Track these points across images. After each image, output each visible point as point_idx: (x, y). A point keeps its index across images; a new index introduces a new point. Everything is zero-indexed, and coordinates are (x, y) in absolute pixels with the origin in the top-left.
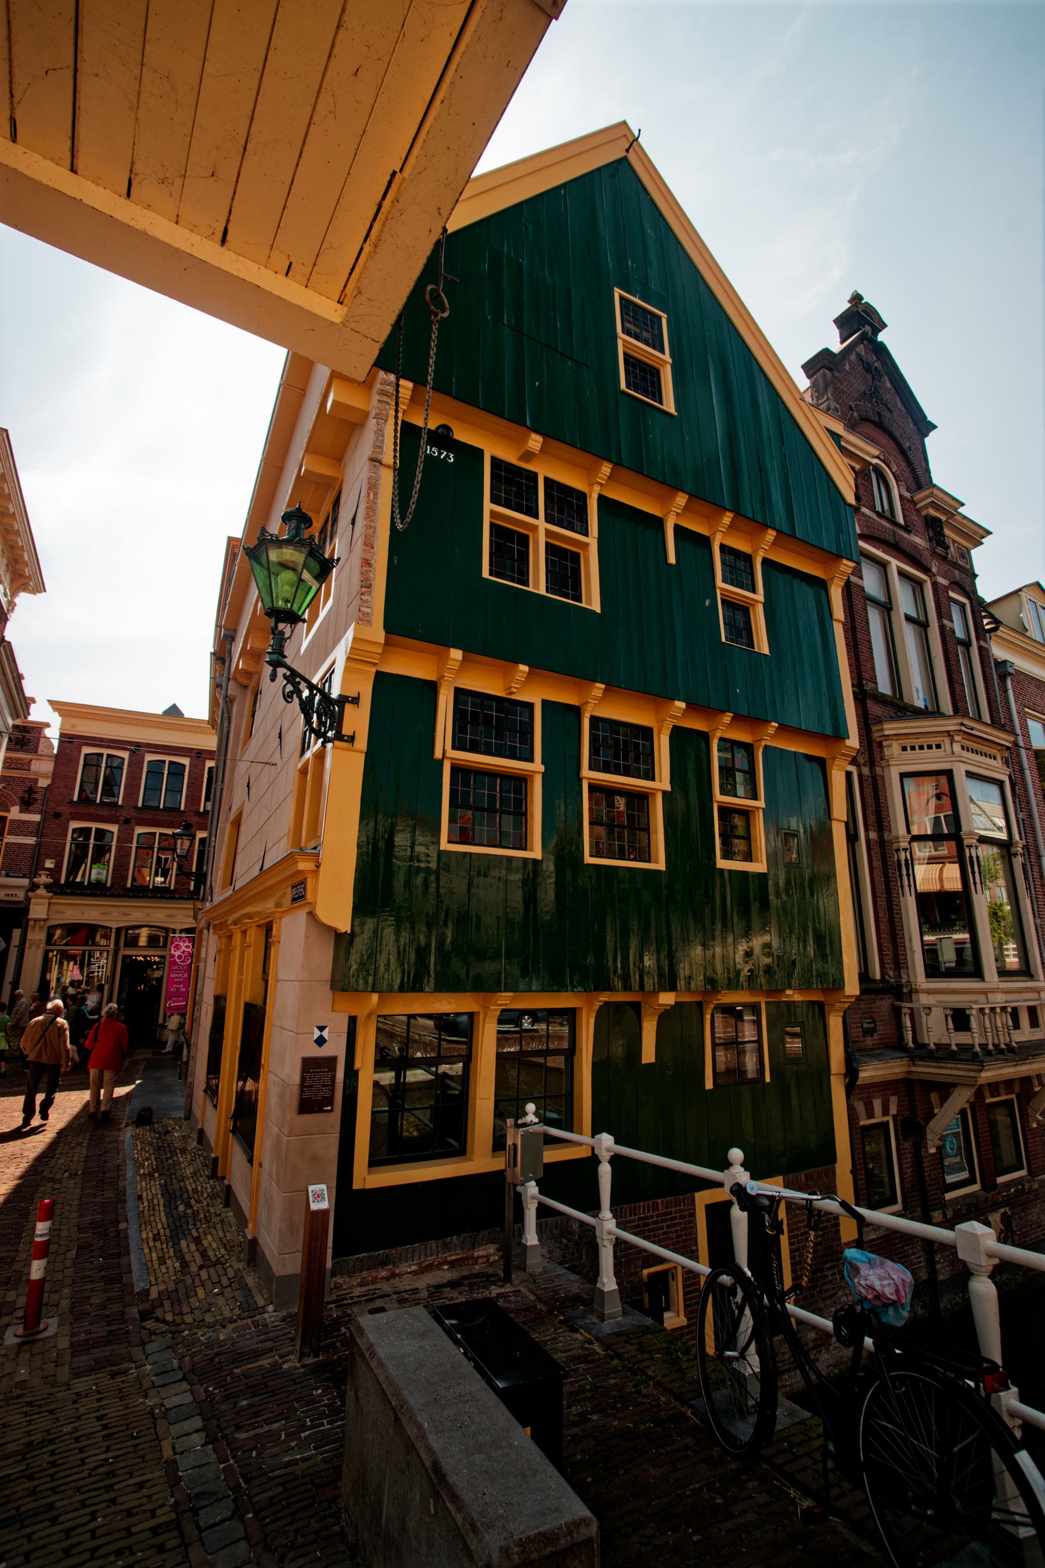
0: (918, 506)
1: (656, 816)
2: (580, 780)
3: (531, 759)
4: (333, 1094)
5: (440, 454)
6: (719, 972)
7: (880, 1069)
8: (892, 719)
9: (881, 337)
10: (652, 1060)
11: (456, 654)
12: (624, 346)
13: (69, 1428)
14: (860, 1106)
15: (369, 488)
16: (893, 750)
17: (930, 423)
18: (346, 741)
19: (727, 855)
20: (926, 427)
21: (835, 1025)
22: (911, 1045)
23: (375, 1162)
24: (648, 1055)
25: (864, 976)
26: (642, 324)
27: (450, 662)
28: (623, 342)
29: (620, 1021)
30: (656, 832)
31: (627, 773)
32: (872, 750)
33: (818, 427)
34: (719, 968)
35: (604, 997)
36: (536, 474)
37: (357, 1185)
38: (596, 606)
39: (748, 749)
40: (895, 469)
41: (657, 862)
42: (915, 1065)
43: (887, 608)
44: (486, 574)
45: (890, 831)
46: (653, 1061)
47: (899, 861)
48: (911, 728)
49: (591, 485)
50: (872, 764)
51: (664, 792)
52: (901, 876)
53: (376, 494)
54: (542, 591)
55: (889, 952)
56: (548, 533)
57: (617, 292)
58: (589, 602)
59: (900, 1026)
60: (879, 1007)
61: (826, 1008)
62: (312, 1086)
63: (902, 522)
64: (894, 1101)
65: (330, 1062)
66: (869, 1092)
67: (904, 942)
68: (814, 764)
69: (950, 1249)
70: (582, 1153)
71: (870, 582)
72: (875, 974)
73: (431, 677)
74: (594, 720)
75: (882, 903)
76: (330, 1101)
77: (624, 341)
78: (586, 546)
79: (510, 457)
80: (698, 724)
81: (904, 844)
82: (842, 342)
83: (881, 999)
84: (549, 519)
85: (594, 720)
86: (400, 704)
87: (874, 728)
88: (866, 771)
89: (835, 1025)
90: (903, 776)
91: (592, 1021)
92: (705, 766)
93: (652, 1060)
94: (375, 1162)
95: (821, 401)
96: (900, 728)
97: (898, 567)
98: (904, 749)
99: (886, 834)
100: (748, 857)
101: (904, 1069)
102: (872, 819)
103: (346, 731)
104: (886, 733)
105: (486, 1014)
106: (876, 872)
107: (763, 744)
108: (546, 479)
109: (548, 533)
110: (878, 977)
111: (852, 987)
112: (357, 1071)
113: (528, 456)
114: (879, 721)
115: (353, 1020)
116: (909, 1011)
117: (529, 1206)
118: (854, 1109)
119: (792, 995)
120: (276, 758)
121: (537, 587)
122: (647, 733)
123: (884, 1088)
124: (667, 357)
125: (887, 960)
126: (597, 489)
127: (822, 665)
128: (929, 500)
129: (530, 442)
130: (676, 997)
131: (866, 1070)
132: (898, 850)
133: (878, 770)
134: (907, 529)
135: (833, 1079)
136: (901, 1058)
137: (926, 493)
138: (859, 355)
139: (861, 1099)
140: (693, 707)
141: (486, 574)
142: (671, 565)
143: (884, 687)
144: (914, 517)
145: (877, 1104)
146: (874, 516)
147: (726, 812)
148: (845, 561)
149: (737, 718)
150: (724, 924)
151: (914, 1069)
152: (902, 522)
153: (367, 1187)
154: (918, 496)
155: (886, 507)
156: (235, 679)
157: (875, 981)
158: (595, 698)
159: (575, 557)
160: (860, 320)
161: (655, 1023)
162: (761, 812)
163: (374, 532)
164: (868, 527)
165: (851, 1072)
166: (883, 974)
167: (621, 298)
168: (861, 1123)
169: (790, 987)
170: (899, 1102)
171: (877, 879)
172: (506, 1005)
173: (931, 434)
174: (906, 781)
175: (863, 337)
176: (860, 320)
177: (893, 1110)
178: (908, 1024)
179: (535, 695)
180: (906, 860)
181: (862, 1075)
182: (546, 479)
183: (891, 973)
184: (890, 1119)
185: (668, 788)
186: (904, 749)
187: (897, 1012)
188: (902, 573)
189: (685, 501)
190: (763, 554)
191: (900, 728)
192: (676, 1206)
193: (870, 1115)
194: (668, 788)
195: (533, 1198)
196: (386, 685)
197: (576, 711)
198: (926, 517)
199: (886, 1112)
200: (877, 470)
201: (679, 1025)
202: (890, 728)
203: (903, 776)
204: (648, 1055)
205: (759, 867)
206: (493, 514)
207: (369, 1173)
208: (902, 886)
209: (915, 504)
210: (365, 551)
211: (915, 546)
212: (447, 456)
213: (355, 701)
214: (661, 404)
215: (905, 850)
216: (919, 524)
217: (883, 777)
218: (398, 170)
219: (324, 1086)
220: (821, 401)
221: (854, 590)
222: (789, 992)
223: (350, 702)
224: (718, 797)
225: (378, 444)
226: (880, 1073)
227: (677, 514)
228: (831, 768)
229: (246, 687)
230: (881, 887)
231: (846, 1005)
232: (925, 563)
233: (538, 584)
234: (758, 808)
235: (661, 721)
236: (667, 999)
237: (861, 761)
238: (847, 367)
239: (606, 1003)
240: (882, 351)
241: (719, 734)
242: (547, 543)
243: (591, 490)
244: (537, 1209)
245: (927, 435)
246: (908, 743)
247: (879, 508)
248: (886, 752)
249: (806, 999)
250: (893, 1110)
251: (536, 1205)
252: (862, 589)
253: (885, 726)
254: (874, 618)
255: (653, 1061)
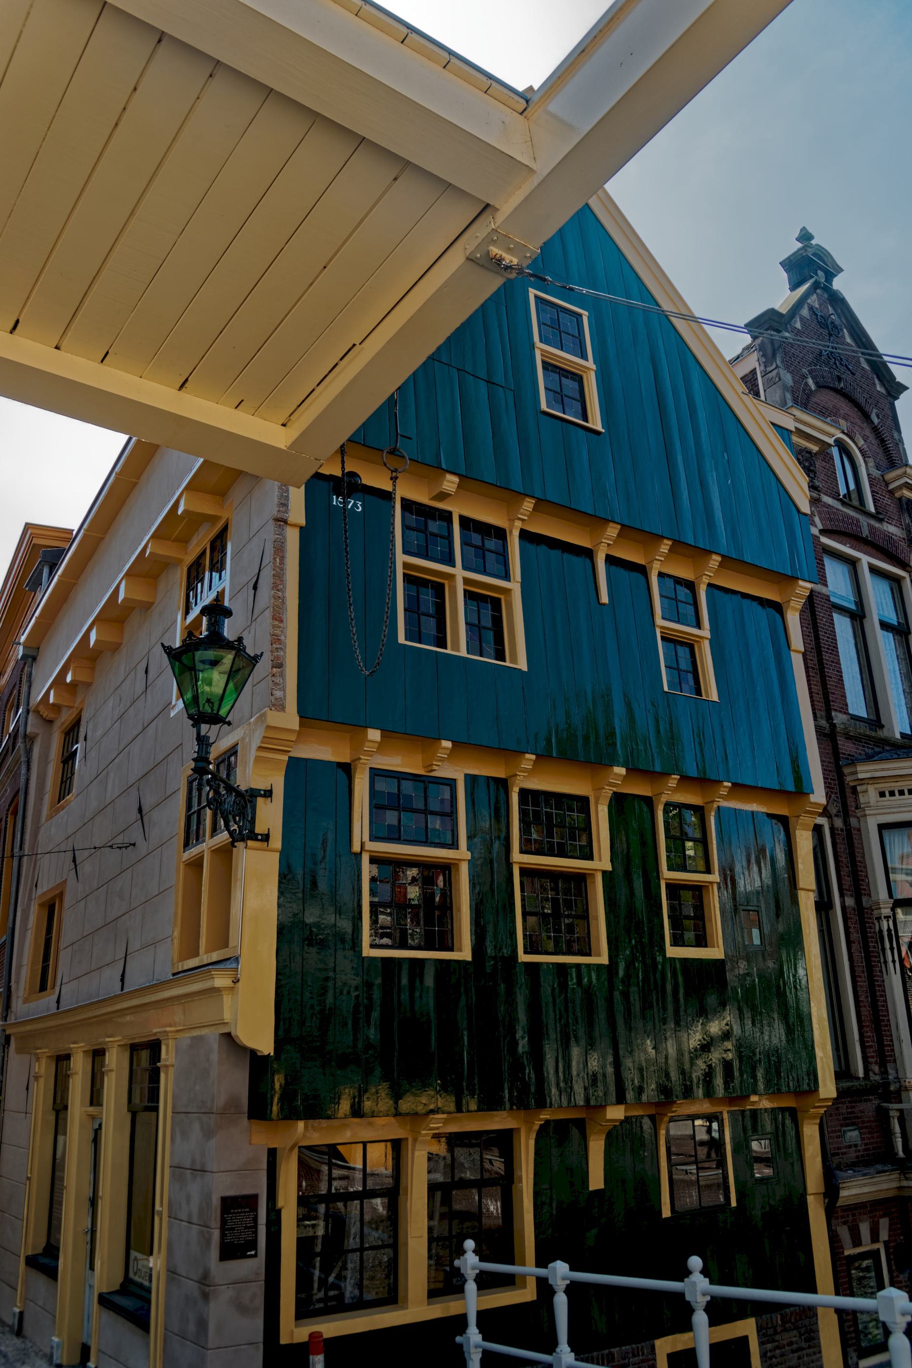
0: (891, 487)
1: (596, 899)
2: (509, 865)
3: (454, 845)
4: (256, 1237)
5: (345, 503)
6: (673, 1079)
7: (865, 1185)
8: (869, 758)
9: (838, 284)
10: (601, 1186)
11: (374, 735)
12: (542, 355)
13: (794, 1075)
14: (844, 1233)
15: (275, 553)
16: (870, 796)
17: (899, 384)
18: (261, 840)
19: (678, 941)
20: (895, 389)
21: (811, 1133)
22: (901, 1154)
23: (304, 1312)
24: (596, 1181)
25: (843, 1073)
26: (560, 329)
27: (367, 744)
28: (542, 349)
29: (561, 1139)
30: (596, 918)
31: (562, 854)
32: (843, 794)
33: (764, 421)
34: (674, 1075)
35: (545, 1116)
36: (450, 513)
37: (284, 1341)
38: (523, 665)
39: (699, 811)
40: (861, 442)
41: (599, 955)
42: (907, 1179)
43: (858, 616)
44: (401, 639)
45: (869, 895)
46: (603, 1187)
47: (881, 931)
48: (888, 769)
49: (511, 520)
50: (845, 813)
51: (604, 873)
52: (884, 950)
53: (282, 558)
54: (463, 653)
55: (873, 1044)
56: (466, 581)
57: (532, 292)
58: (514, 660)
59: (888, 1134)
60: (861, 1112)
61: (799, 1115)
62: (233, 1229)
63: (873, 510)
64: (884, 1223)
65: (251, 1201)
66: (854, 1215)
67: (890, 1030)
68: (774, 821)
69: (873, 1314)
70: (527, 1294)
71: (837, 583)
72: (857, 1071)
73: (346, 759)
74: (524, 793)
75: (863, 983)
76: (253, 1245)
77: (542, 350)
78: (507, 591)
79: (421, 497)
80: (640, 789)
81: (886, 911)
82: (793, 288)
83: (866, 1101)
84: (465, 568)
85: (524, 793)
86: (315, 790)
87: (846, 771)
88: (839, 823)
89: (811, 1133)
90: (882, 827)
91: (532, 1142)
92: (650, 842)
93: (601, 1186)
94: (304, 1312)
95: (769, 369)
96: (876, 770)
97: (869, 564)
98: (882, 794)
99: (864, 899)
100: (702, 941)
101: (895, 1185)
102: (847, 881)
103: (259, 829)
104: (861, 776)
105: (415, 1140)
106: (855, 947)
107: (715, 806)
108: (462, 518)
109: (466, 581)
110: (861, 1074)
111: (828, 1088)
112: (280, 1211)
113: (442, 496)
114: (853, 761)
115: (272, 1154)
116: (897, 1114)
117: (473, 1356)
118: (837, 1235)
119: (763, 1103)
120: (135, 834)
121: (456, 647)
122: (583, 803)
123: (873, 1208)
124: (590, 364)
125: (871, 1052)
126: (518, 524)
127: (778, 702)
128: (902, 481)
129: (445, 483)
130: (626, 1111)
131: (849, 1188)
132: (879, 919)
133: (853, 821)
134: (877, 517)
135: (810, 1199)
136: (892, 1170)
137: (899, 472)
138: (811, 308)
139: (845, 1223)
140: (634, 771)
141: (401, 639)
142: (604, 604)
143: (857, 705)
144: (887, 501)
145: (865, 1229)
146: (837, 505)
147: (674, 889)
148: (801, 583)
149: (685, 779)
150: (677, 1023)
151: (905, 1183)
152: (873, 510)
153: (295, 1341)
154: (890, 476)
155: (852, 486)
156: (37, 712)
157: (858, 1078)
158: (525, 770)
159: (496, 604)
160: (810, 266)
161: (603, 1142)
162: (715, 886)
163: (283, 603)
164: (831, 520)
165: (831, 1191)
166: (866, 1070)
167: (536, 297)
168: (847, 1253)
169: (755, 1092)
170: (890, 1224)
171: (856, 955)
172: (438, 1128)
173: (902, 396)
174: (886, 833)
175: (816, 286)
176: (810, 266)
177: (884, 1235)
178: (897, 1129)
179: (457, 771)
180: (889, 930)
181: (843, 1193)
182: (462, 518)
183: (876, 1068)
184: (880, 1246)
185: (609, 867)
186: (882, 794)
187: (883, 1116)
188: (874, 570)
189: (617, 531)
190: (707, 581)
191: (876, 770)
192: (634, 1356)
193: (857, 1242)
194: (609, 867)
195: (477, 1347)
196: (298, 770)
197: (502, 785)
198: (900, 499)
199: (875, 1238)
200: (839, 443)
201: (626, 1141)
202: (864, 771)
203: (882, 827)
204: (596, 1181)
205: (715, 952)
206: (406, 565)
207: (296, 1326)
208: (886, 962)
209: (887, 484)
210: (274, 626)
211: (889, 537)
212: (355, 505)
213: (268, 794)
214: (587, 421)
215: (887, 918)
216: (893, 508)
217: (859, 830)
218: (357, 344)
219: (246, 1228)
220: (769, 369)
221: (817, 600)
222: (754, 1098)
223: (261, 796)
224: (667, 874)
225: (283, 501)
226: (866, 1190)
227: (609, 545)
228: (795, 829)
229: (50, 722)
230: (861, 965)
231: (822, 1111)
232: (902, 556)
233: (459, 645)
234: (711, 883)
235: (598, 789)
236: (616, 1113)
237: (833, 810)
238: (798, 325)
239: (547, 1122)
240: (837, 300)
241: (664, 799)
242: (465, 591)
243: (512, 527)
244: (482, 1360)
245: (897, 398)
246: (886, 786)
247: (843, 491)
248: (862, 799)
249: (775, 1105)
250: (884, 1235)
251: (480, 1356)
252: (827, 598)
253: (859, 768)
254: (843, 627)
255: (603, 1187)
